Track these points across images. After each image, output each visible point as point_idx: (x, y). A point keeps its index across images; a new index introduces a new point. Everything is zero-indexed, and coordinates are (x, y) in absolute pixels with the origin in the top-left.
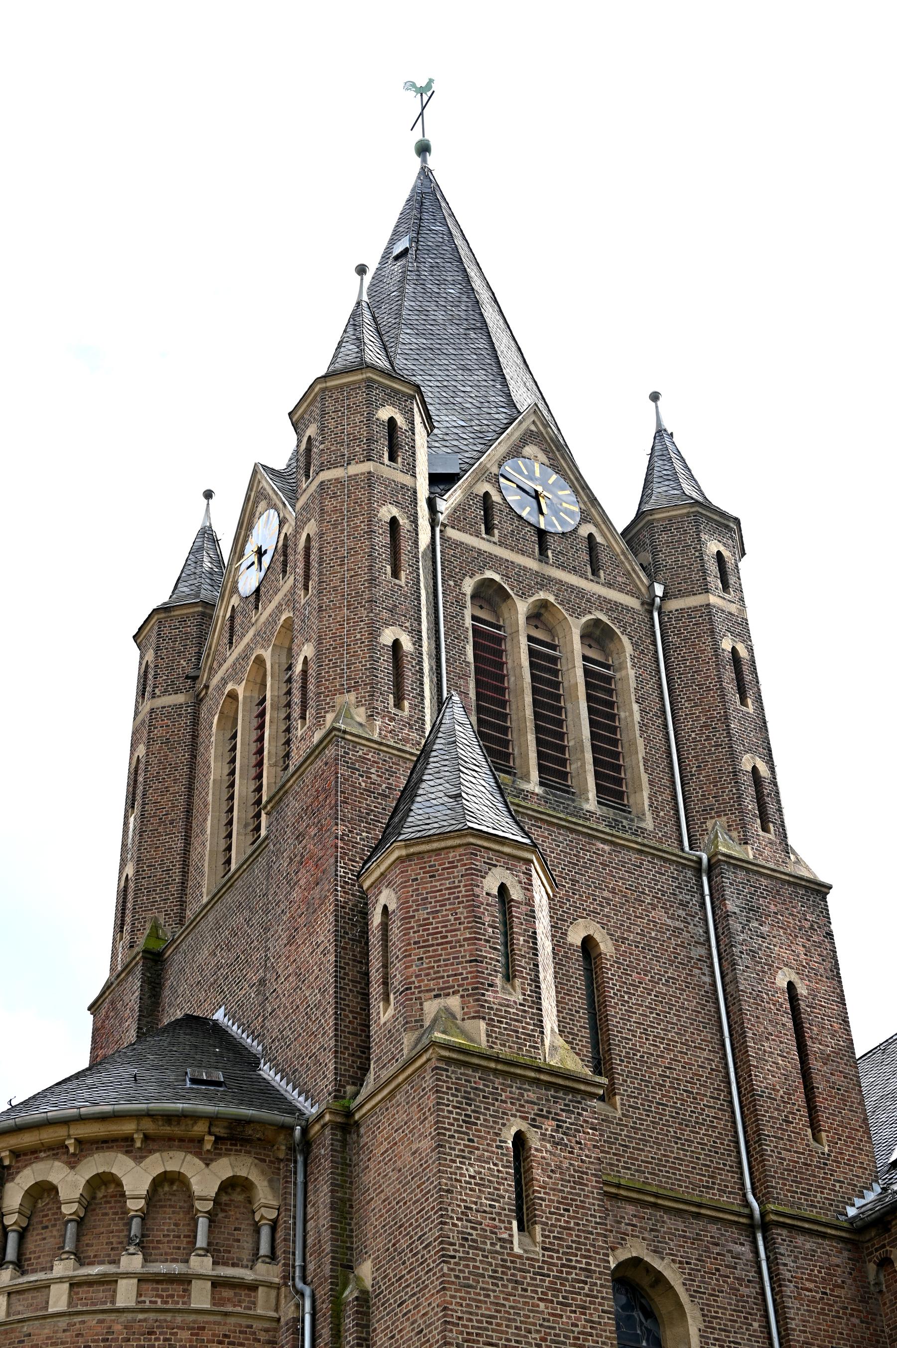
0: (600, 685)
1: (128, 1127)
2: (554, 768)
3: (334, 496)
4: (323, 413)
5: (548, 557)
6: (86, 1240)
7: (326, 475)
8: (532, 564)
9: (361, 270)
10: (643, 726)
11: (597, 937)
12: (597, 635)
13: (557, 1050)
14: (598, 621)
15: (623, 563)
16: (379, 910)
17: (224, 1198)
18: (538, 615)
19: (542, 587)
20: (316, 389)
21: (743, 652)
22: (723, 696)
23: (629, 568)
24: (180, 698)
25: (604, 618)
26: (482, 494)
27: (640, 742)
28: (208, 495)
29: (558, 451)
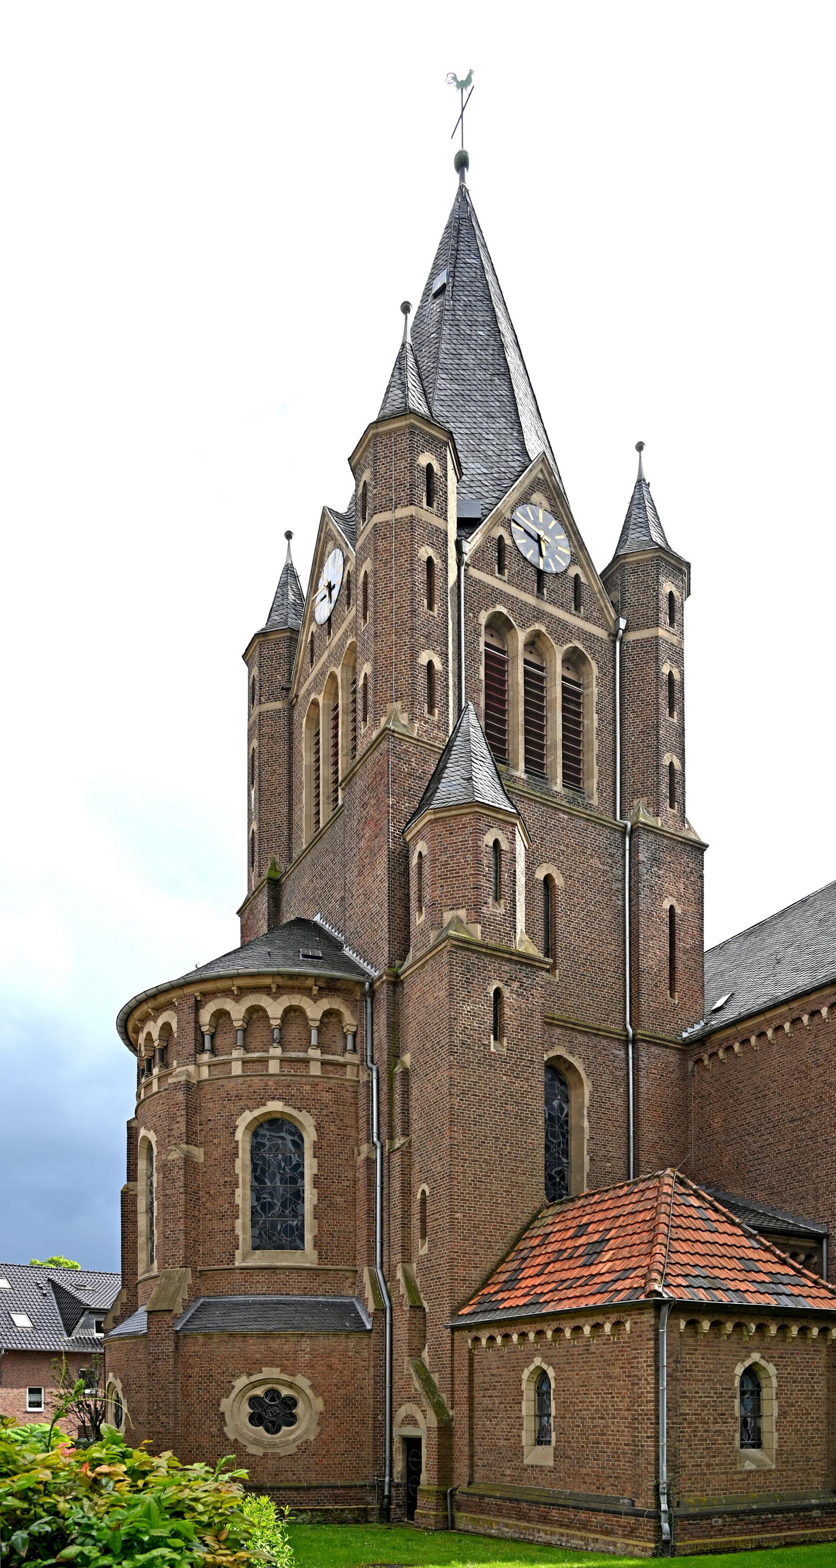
0: (573, 699)
1: (267, 981)
2: (535, 762)
4: (376, 459)
6: (249, 1040)
8: (531, 600)
10: (599, 730)
12: (574, 659)
13: (523, 942)
15: (598, 600)
16: (416, 855)
17: (326, 1020)
19: (537, 619)
21: (676, 676)
24: (278, 705)
25: (580, 646)
27: (596, 743)
28: (640, 447)
29: (559, 498)
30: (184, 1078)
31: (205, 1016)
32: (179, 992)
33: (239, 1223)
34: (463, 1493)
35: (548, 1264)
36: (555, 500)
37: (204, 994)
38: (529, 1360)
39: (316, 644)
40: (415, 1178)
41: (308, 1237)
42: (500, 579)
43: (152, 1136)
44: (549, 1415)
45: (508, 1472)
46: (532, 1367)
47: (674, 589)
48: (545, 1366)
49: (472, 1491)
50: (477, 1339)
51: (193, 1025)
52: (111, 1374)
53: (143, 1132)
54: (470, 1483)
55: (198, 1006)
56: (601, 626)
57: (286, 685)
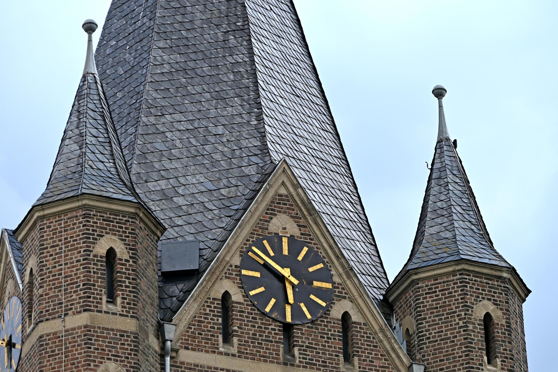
4: (42, 248)
5: (293, 356)
7: (45, 328)
9: (89, 27)
15: (381, 341)
20: (35, 217)
23: (388, 347)
26: (220, 296)
28: (439, 93)
29: (311, 215)
36: (306, 218)
42: (227, 354)
47: (490, 307)
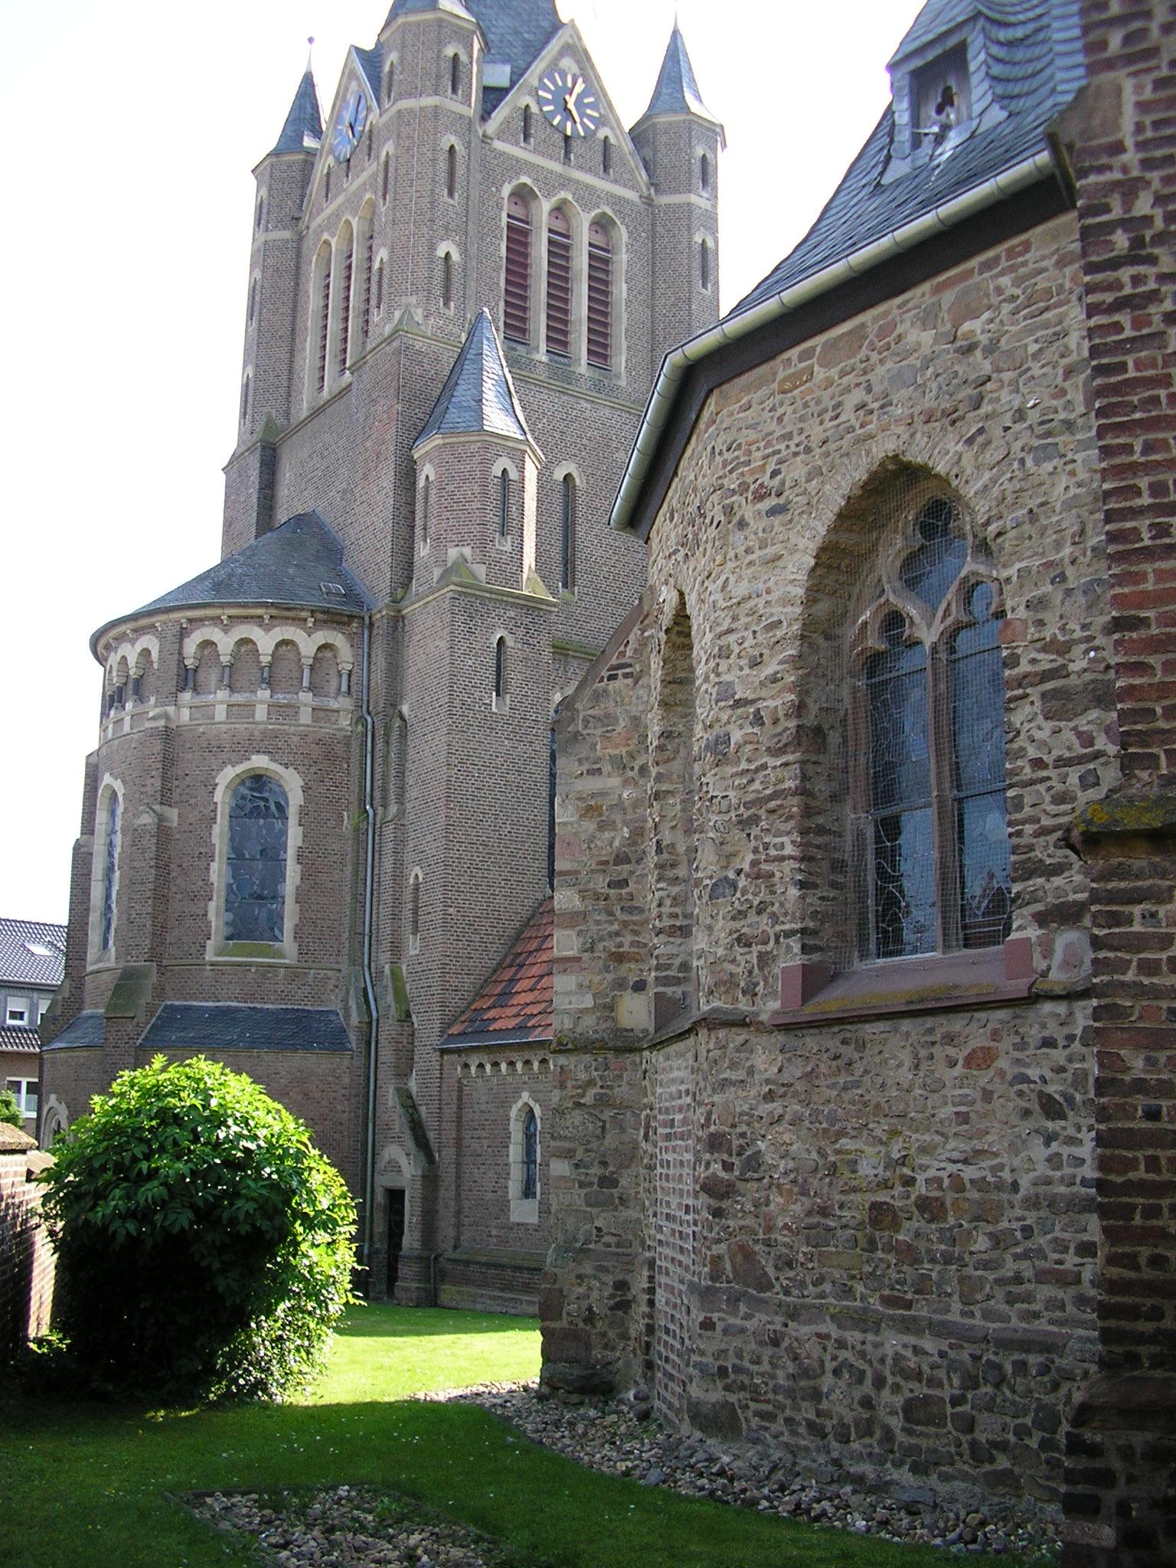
0: (600, 264)
1: (260, 611)
2: (559, 336)
3: (409, 124)
6: (235, 677)
7: (405, 104)
8: (556, 167)
10: (628, 301)
11: (575, 475)
12: (602, 224)
13: (530, 582)
14: (604, 214)
16: (423, 477)
17: (320, 655)
18: (559, 210)
19: (563, 186)
21: (710, 244)
22: (689, 282)
24: (287, 234)
25: (610, 212)
27: (624, 316)
28: (311, 40)
30: (162, 723)
31: (191, 646)
32: (164, 617)
33: (212, 906)
34: (448, 1260)
35: (542, 976)
37: (190, 620)
38: (516, 1094)
39: (332, 180)
40: (408, 857)
41: (289, 925)
43: (118, 786)
44: (535, 1162)
45: (494, 1232)
46: (520, 1104)
48: (532, 1103)
49: (457, 1257)
50: (466, 1066)
51: (176, 657)
52: (53, 1097)
53: (107, 779)
54: (455, 1247)
55: (183, 634)
56: (633, 188)
57: (297, 215)
